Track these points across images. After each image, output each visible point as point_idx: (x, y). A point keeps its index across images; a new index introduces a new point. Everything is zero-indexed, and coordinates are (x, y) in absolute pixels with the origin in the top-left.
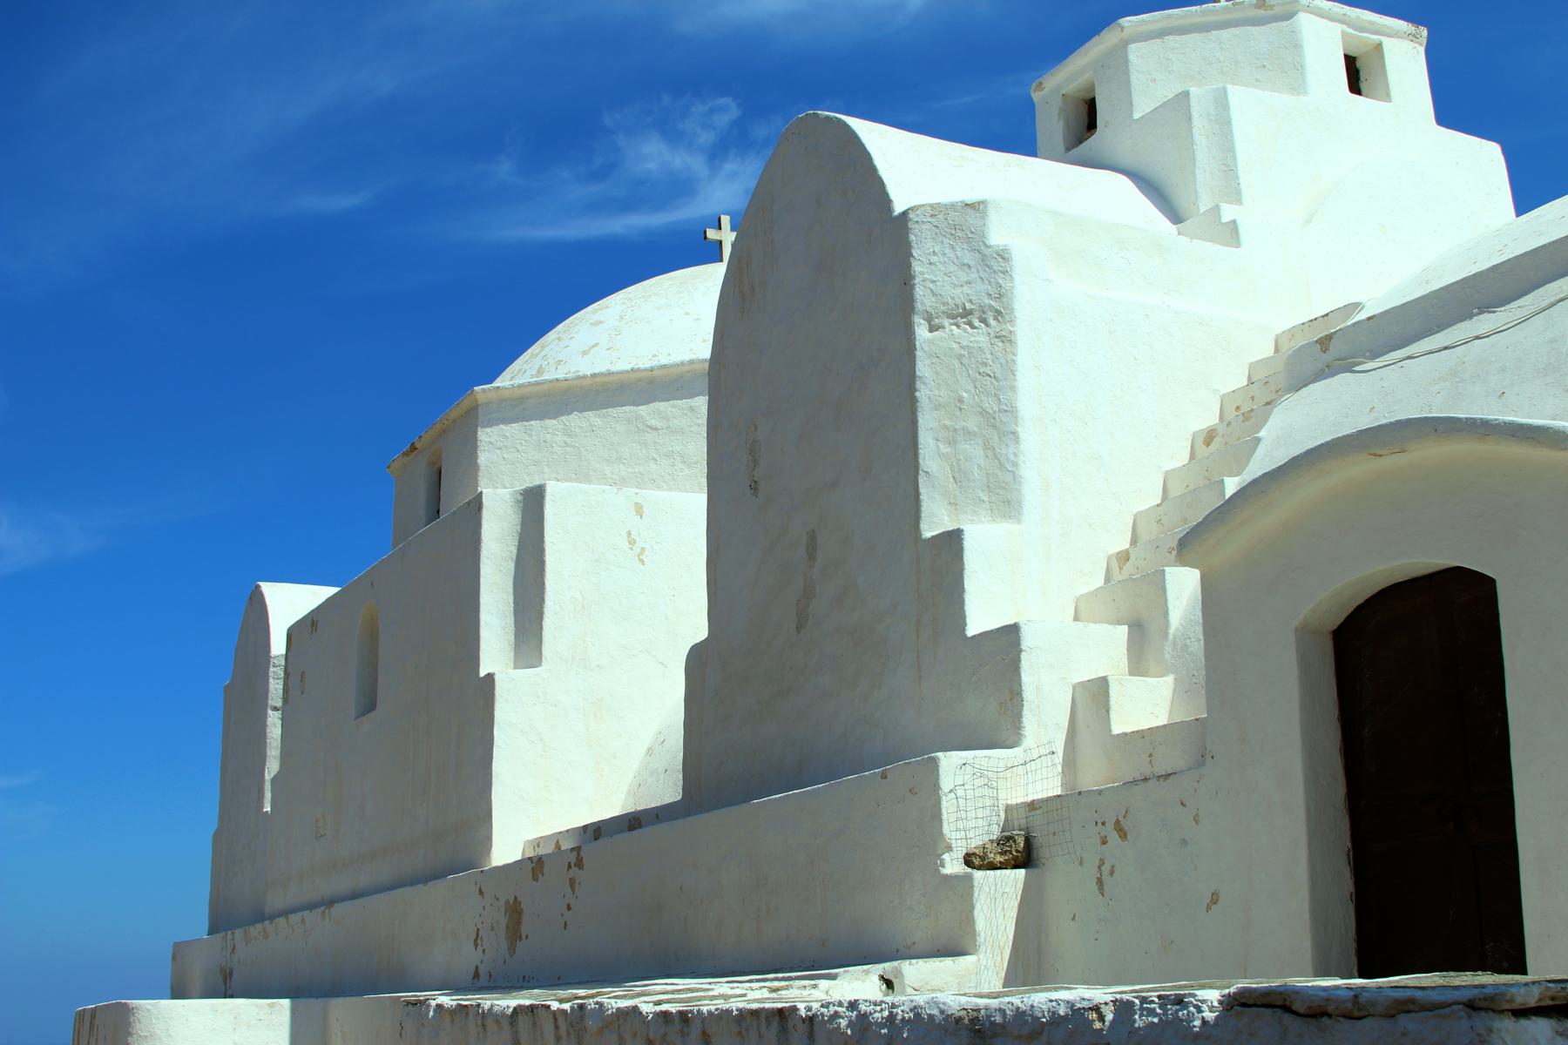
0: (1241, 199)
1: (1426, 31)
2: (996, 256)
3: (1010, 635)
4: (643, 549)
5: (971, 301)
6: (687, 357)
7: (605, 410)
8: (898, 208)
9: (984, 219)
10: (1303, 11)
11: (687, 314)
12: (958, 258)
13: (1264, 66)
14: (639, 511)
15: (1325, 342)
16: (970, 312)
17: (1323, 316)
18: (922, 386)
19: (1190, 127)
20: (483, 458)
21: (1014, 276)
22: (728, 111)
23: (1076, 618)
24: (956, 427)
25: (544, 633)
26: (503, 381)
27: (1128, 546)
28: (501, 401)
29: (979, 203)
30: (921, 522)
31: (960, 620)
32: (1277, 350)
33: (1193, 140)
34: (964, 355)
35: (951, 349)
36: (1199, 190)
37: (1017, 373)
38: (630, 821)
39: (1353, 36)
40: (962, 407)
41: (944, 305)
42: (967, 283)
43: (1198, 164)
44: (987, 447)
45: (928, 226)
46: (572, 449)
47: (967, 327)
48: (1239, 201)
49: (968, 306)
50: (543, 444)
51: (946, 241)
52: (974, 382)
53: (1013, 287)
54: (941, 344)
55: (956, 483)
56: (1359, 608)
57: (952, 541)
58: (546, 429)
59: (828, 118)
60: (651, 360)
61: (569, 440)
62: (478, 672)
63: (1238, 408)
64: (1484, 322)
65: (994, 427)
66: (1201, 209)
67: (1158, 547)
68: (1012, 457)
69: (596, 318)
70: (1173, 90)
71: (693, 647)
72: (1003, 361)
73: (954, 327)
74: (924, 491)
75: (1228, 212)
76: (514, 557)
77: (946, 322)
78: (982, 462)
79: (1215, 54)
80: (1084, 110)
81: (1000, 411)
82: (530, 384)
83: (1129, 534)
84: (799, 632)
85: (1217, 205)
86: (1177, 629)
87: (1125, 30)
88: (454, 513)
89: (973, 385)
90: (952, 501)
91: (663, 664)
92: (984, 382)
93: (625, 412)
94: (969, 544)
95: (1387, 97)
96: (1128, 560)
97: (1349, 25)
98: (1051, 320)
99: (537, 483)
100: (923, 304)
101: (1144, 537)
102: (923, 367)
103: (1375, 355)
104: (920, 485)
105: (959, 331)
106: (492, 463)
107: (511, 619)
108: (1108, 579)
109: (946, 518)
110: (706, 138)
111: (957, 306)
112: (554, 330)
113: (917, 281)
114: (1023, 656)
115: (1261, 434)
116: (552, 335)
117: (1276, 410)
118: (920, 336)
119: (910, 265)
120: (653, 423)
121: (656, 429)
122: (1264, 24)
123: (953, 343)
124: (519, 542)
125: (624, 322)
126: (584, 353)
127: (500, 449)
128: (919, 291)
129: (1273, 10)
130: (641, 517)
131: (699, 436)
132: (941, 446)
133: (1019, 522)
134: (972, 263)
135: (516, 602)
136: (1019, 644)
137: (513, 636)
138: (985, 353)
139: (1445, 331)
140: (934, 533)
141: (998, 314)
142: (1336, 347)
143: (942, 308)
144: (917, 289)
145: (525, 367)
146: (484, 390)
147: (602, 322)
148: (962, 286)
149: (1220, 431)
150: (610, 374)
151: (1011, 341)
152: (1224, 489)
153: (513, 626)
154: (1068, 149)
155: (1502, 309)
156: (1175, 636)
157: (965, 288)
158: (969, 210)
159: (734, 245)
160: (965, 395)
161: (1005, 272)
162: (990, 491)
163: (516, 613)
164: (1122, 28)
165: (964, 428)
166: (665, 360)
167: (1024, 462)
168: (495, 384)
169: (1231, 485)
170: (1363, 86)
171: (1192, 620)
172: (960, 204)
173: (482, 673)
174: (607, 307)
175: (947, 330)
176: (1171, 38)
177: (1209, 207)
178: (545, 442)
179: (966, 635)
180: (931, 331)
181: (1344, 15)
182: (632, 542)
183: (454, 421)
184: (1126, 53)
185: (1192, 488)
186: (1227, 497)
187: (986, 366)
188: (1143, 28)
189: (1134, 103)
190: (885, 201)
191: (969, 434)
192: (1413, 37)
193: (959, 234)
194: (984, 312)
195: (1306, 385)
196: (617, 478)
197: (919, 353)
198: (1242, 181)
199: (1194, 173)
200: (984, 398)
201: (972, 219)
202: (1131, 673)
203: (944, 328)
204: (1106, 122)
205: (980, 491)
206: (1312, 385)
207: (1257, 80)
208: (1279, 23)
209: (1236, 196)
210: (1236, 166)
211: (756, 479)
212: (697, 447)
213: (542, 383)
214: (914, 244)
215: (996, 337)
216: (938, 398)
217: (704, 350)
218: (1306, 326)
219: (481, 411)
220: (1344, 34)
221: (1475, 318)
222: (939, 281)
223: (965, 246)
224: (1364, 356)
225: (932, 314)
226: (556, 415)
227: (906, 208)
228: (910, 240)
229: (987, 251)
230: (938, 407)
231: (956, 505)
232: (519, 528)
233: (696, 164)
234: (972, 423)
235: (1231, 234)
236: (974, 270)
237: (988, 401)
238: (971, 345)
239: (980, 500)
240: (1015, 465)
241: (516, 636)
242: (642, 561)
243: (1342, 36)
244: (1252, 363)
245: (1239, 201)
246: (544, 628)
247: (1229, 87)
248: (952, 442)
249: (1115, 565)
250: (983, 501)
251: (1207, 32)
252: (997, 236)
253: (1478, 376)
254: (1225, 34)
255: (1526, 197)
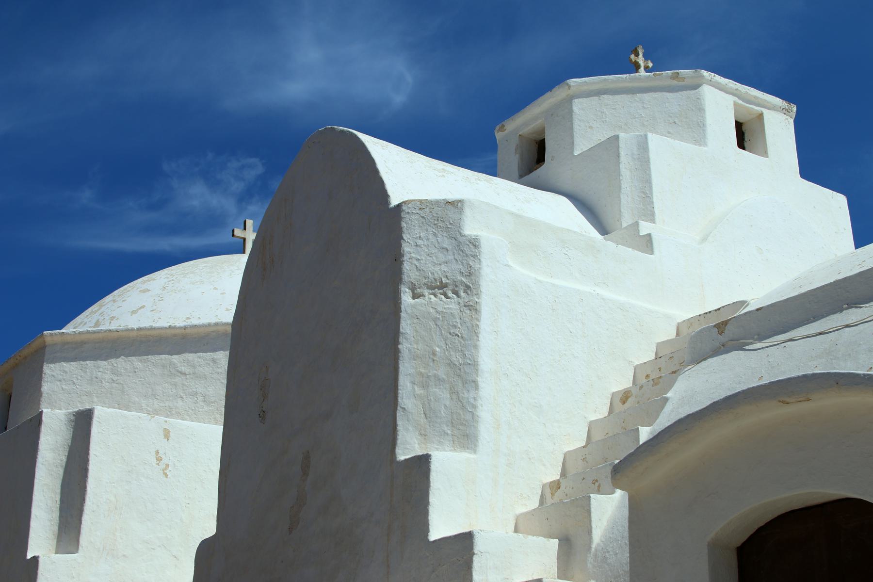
0: (654, 219)
1: (795, 107)
2: (468, 243)
3: (465, 541)
4: (167, 465)
5: (446, 277)
6: (213, 320)
7: (146, 357)
8: (394, 201)
9: (461, 214)
10: (707, 84)
11: (215, 289)
12: (438, 243)
13: (675, 123)
14: (167, 435)
15: (721, 327)
16: (445, 286)
17: (716, 310)
18: (404, 340)
19: (618, 163)
20: (46, 387)
21: (482, 260)
22: (255, 168)
23: (516, 531)
24: (429, 374)
25: (82, 526)
26: (69, 329)
27: (558, 477)
28: (65, 344)
29: (458, 202)
30: (397, 448)
31: (425, 528)
32: (678, 334)
33: (620, 172)
34: (439, 319)
35: (429, 313)
36: (623, 210)
37: (480, 336)
38: (65, 450)
39: (740, 105)
40: (435, 359)
41: (425, 278)
42: (444, 262)
43: (623, 191)
44: (453, 392)
45: (417, 217)
46: (117, 385)
47: (443, 297)
48: (653, 221)
49: (444, 280)
50: (95, 379)
51: (430, 229)
52: (445, 340)
53: (480, 268)
54: (422, 309)
55: (426, 419)
56: (760, 530)
57: (422, 463)
58: (98, 367)
59: (342, 131)
60: (185, 321)
61: (115, 378)
62: (26, 555)
63: (647, 376)
64: (853, 315)
65: (459, 376)
66: (623, 224)
67: (584, 479)
68: (472, 401)
69: (145, 287)
70: (605, 135)
71: (203, 542)
72: (469, 325)
73: (432, 297)
74: (400, 423)
75: (645, 228)
76: (64, 465)
77: (426, 292)
78: (448, 403)
79: (638, 111)
80: (535, 148)
81: (464, 364)
82: (88, 332)
83: (560, 468)
84: (290, 532)
85: (637, 221)
86: (598, 545)
87: (572, 88)
88: (18, 428)
89: (444, 342)
90: (423, 432)
91: (175, 557)
92: (454, 341)
93: (161, 359)
94: (435, 466)
95: (764, 153)
96: (559, 488)
97: (739, 98)
98: (508, 296)
99: (88, 407)
100: (409, 276)
101: (572, 470)
102: (406, 326)
103: (761, 339)
104: (398, 419)
105: (436, 299)
106: (53, 391)
107: (56, 514)
108: (542, 502)
109: (417, 445)
110: (237, 186)
111: (435, 280)
112: (110, 295)
113: (405, 258)
114: (476, 559)
115: (669, 395)
116: (109, 298)
117: (680, 378)
118: (405, 301)
119: (400, 246)
120: (183, 369)
121: (185, 374)
122: (677, 91)
123: (431, 309)
124: (69, 453)
125: (166, 291)
126: (133, 312)
127: (60, 381)
128: (406, 267)
129: (684, 81)
130: (168, 440)
131: (218, 382)
132: (416, 388)
133: (475, 452)
134: (449, 248)
135: (62, 501)
136: (472, 549)
137: (57, 528)
138: (455, 318)
139: (820, 321)
140: (407, 457)
141: (467, 288)
142: (730, 331)
143: (424, 281)
144: (405, 265)
145: (86, 320)
146: (51, 334)
147: (149, 290)
148: (440, 265)
149: (634, 392)
150: (152, 329)
151: (476, 309)
152: (638, 436)
153: (58, 519)
154: (521, 176)
155: (867, 305)
156: (596, 550)
157: (443, 266)
158: (450, 206)
159: (255, 242)
160: (438, 349)
161: (475, 256)
162: (454, 427)
163: (61, 509)
164: (569, 87)
165: (435, 376)
166: (195, 322)
167: (481, 405)
168: (63, 331)
169: (645, 434)
170: (746, 145)
171: (610, 537)
172: (443, 202)
173: (29, 556)
174: (154, 280)
175: (427, 298)
176: (605, 96)
177: (630, 223)
178: (97, 378)
179: (428, 540)
180: (414, 298)
181: (737, 89)
182: (159, 459)
183: (25, 358)
184: (571, 105)
185: (611, 434)
186: (641, 443)
187: (456, 328)
188: (585, 88)
189: (575, 143)
190: (384, 195)
191: (439, 380)
192: (786, 111)
193: (441, 224)
194: (456, 286)
195: (705, 359)
196: (151, 410)
197: (403, 315)
198: (656, 206)
199: (620, 197)
200: (452, 353)
201: (451, 213)
202: (559, 578)
203: (424, 296)
204: (552, 156)
205: (445, 426)
206: (710, 360)
207: (669, 133)
208: (688, 91)
209: (651, 217)
210: (651, 193)
211: (264, 409)
212: (218, 390)
213: (98, 332)
214: (404, 230)
215: (465, 306)
216: (416, 350)
217: (229, 317)
218: (702, 318)
219: (47, 349)
220: (735, 104)
221: (844, 311)
222: (422, 259)
223: (445, 234)
224: (753, 338)
225: (415, 285)
226: (106, 358)
227: (399, 202)
228: (402, 226)
229: (461, 239)
230: (415, 357)
231: (425, 435)
232: (69, 442)
233: (229, 205)
234: (442, 372)
235: (647, 244)
236: (450, 253)
237: (456, 355)
238: (445, 311)
239: (445, 433)
240: (475, 407)
241: (60, 528)
242: (166, 475)
243: (734, 105)
244: (659, 343)
245: (653, 221)
246: (83, 522)
247: (650, 135)
248: (425, 386)
249: (548, 492)
250: (447, 434)
251: (633, 94)
252: (470, 229)
253: (850, 355)
254: (647, 97)
255: (860, 241)
